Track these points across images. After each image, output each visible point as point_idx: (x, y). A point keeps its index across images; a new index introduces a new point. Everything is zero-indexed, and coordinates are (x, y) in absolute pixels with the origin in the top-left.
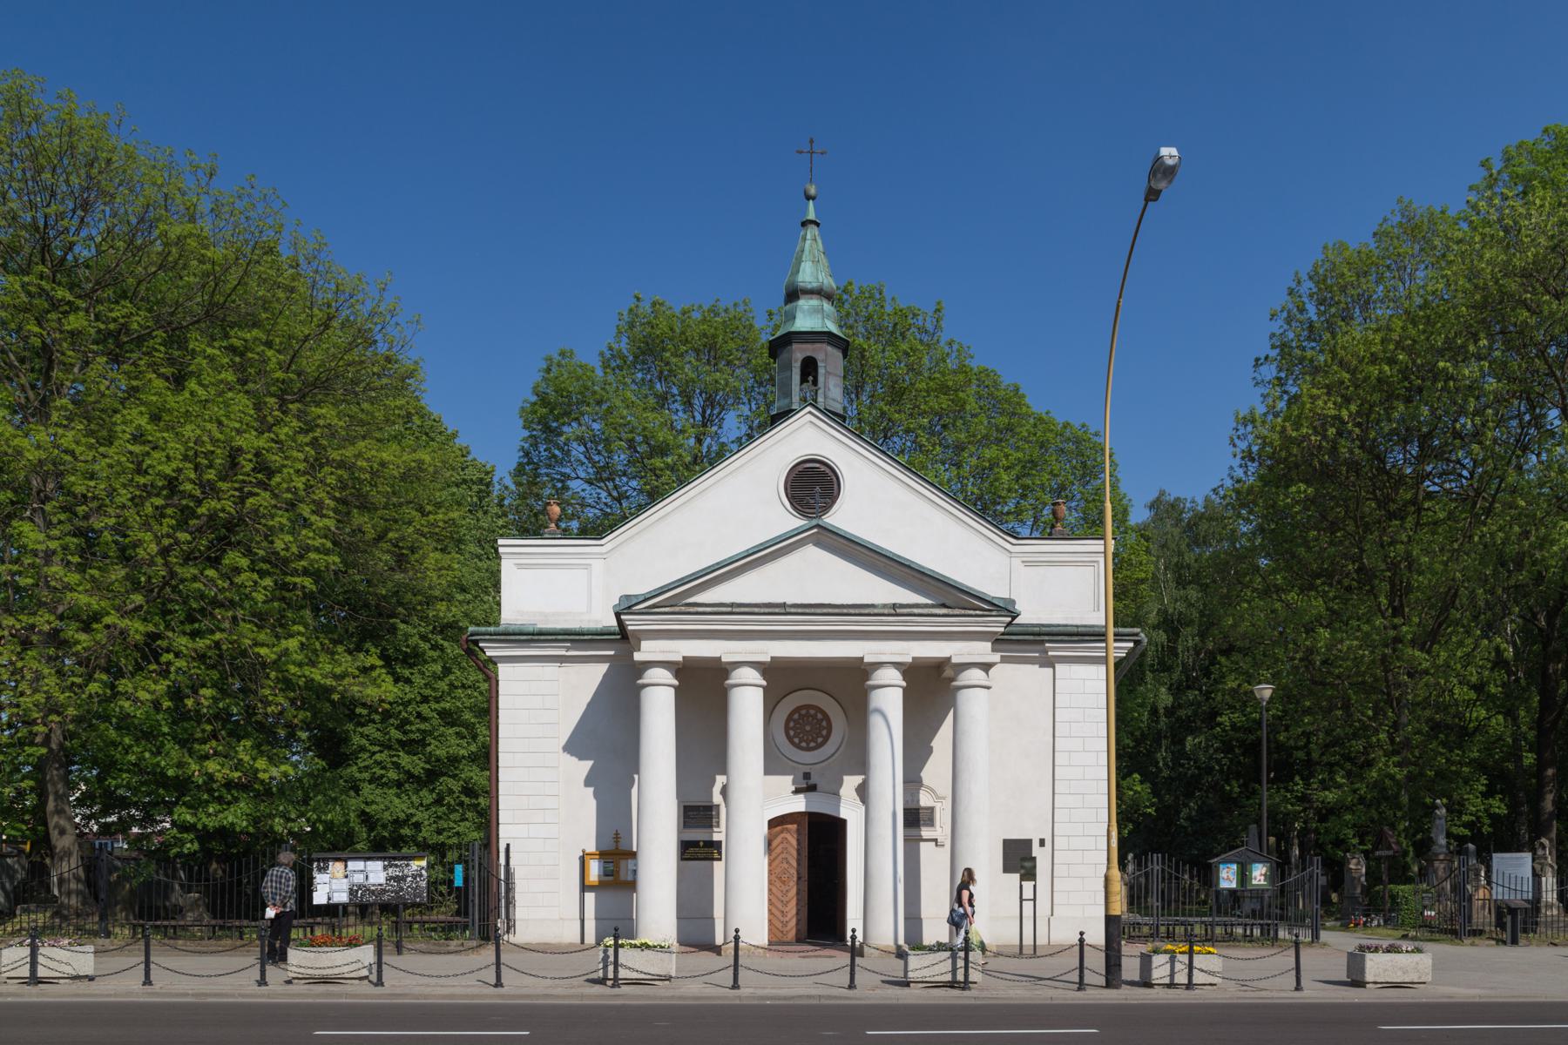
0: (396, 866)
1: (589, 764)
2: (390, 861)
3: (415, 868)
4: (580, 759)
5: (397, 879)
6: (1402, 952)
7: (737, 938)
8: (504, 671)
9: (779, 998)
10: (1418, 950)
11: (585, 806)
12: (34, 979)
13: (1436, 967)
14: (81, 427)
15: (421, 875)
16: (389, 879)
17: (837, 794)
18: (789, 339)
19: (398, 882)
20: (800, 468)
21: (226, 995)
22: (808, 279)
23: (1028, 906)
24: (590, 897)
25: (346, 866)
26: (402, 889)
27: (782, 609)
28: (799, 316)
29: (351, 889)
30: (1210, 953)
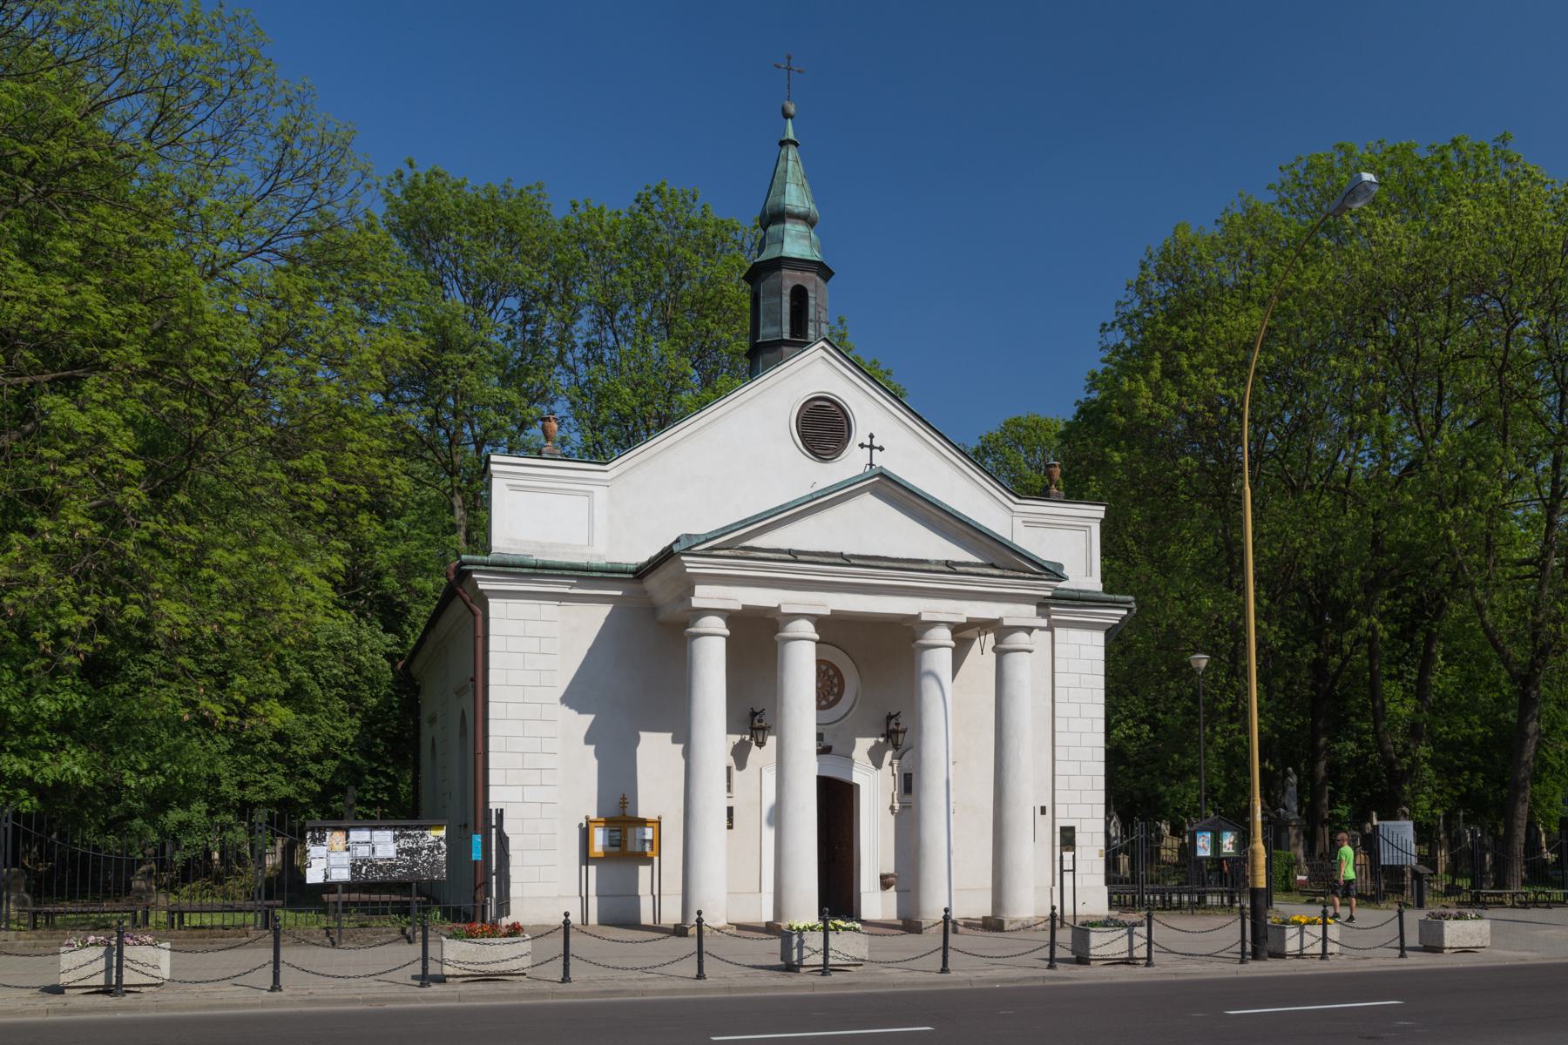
0: (409, 836)
1: (590, 718)
2: (401, 831)
3: (431, 838)
4: (581, 712)
5: (410, 852)
6: (1467, 919)
7: (700, 921)
8: (494, 605)
9: (1008, 981)
10: (1479, 917)
11: (586, 766)
12: (425, 979)
13: (1493, 932)
14: (99, 281)
15: (439, 847)
16: (400, 852)
17: (849, 757)
18: (780, 263)
19: (412, 855)
20: (811, 405)
21: (236, 1006)
22: (795, 203)
23: (1068, 877)
24: (592, 869)
25: (347, 837)
26: (416, 864)
27: (845, 559)
28: (787, 240)
29: (353, 865)
30: (856, 930)
